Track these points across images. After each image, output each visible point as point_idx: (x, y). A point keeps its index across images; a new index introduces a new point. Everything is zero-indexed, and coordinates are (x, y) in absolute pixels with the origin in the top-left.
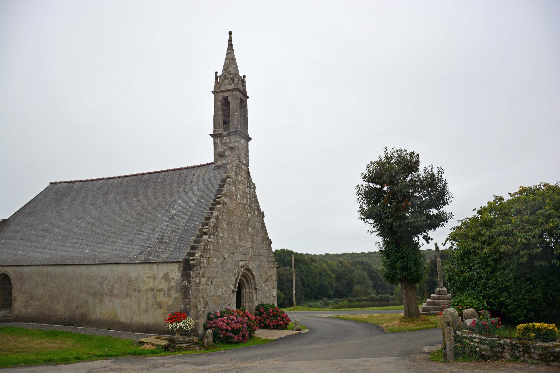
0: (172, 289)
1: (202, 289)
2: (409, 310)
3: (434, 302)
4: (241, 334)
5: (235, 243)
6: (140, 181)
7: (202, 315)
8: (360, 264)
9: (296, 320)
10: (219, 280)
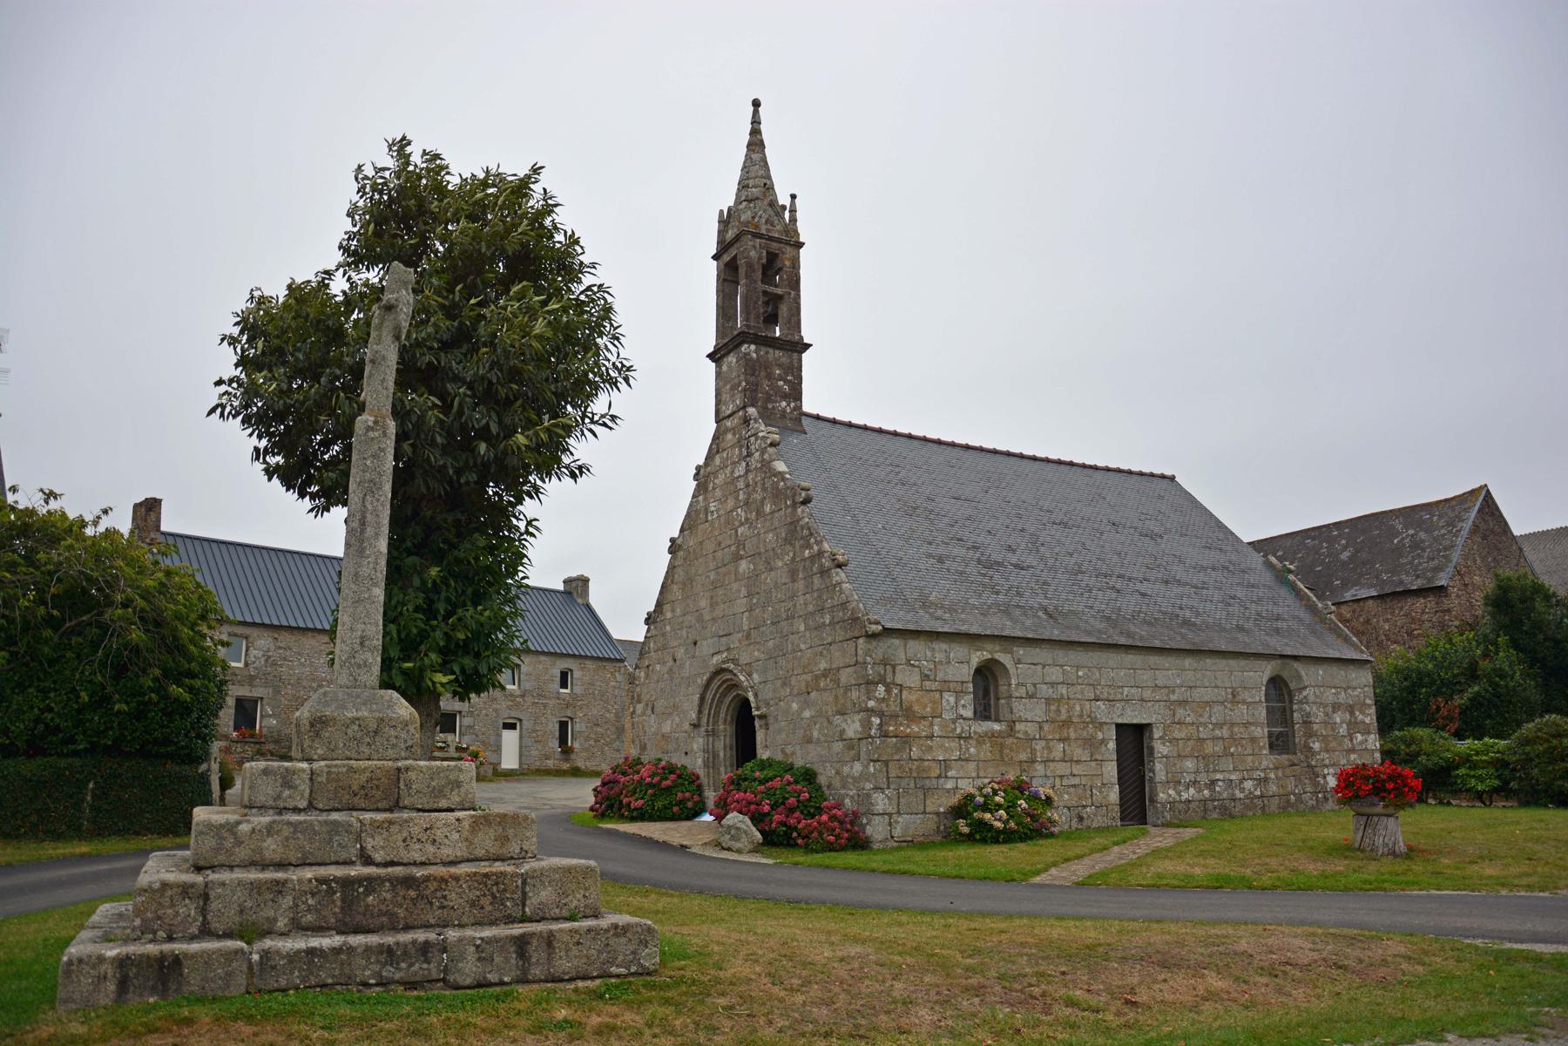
1: (638, 722)
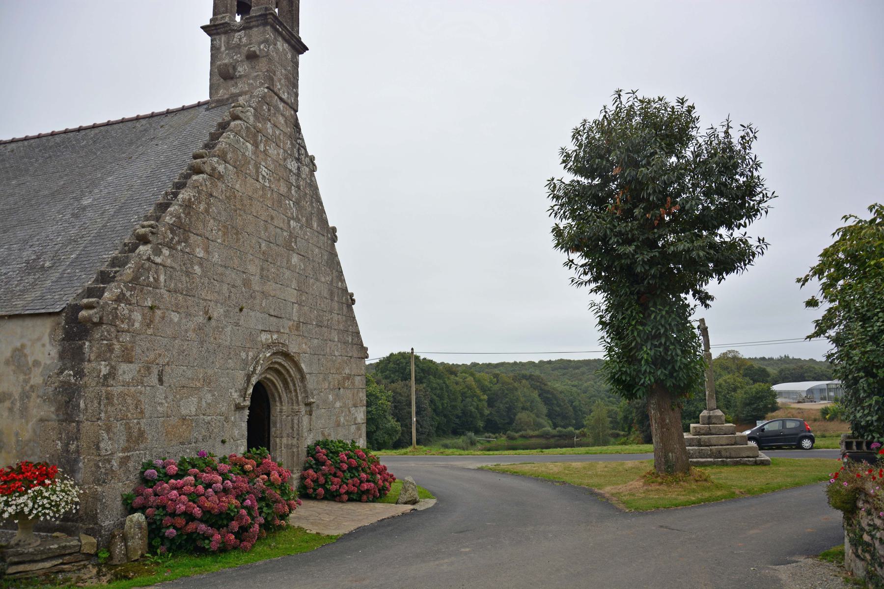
0: (34, 395)
1: (122, 395)
2: (666, 456)
3: (700, 439)
4: (235, 525)
5: (247, 283)
6: (41, 148)
7: (120, 472)
8: (527, 379)
9: (406, 479)
10: (189, 373)
